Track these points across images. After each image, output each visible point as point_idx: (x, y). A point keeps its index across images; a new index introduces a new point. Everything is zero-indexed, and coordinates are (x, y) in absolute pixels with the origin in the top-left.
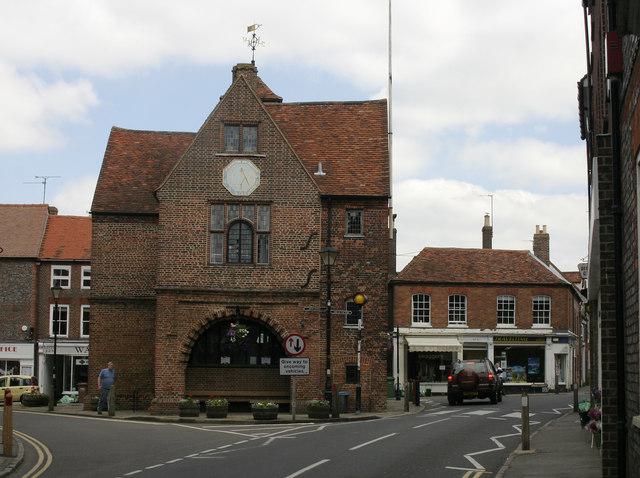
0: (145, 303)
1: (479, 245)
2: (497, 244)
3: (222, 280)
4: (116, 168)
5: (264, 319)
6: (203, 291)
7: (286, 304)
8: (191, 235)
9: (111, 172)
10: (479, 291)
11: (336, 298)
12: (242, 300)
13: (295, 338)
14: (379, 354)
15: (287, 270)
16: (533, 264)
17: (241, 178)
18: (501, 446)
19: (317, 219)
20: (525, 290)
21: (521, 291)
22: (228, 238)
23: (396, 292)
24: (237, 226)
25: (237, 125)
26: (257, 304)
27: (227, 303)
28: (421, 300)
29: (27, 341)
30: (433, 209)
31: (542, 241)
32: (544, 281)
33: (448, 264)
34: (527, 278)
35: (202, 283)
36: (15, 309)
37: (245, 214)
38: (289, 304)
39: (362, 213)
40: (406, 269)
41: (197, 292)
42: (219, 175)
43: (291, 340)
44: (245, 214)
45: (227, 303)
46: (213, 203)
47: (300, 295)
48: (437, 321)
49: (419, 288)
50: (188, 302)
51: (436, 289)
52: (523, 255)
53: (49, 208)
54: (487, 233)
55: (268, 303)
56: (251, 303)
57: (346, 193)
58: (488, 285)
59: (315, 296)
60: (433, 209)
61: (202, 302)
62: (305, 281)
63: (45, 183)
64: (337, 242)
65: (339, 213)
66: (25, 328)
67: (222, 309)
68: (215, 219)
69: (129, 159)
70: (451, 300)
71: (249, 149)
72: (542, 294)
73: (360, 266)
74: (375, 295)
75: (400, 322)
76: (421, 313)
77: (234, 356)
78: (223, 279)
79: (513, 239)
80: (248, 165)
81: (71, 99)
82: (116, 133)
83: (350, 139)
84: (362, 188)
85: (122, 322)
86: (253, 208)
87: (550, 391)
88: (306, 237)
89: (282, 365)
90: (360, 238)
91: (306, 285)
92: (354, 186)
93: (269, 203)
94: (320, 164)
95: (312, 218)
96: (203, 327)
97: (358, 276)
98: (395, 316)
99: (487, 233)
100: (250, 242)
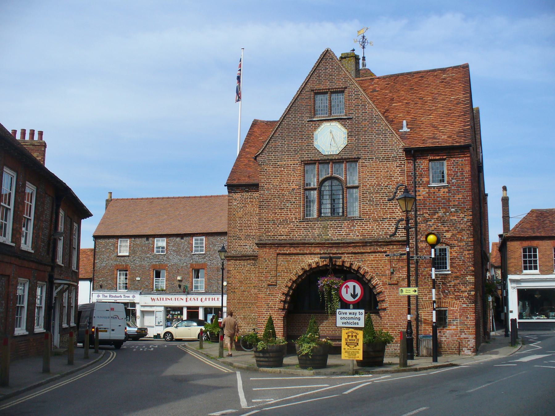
3: (315, 233)
6: (298, 244)
7: (375, 252)
9: (248, 153)
15: (375, 220)
17: (330, 138)
19: (402, 171)
23: (508, 246)
24: (327, 183)
27: (320, 254)
38: (378, 252)
39: (445, 163)
40: (517, 226)
41: (292, 245)
42: (310, 137)
43: (347, 287)
44: (340, 172)
45: (320, 254)
48: (544, 269)
56: (342, 253)
65: (423, 163)
67: (317, 260)
74: (461, 240)
76: (530, 262)
78: (317, 232)
83: (434, 99)
89: (338, 316)
90: (444, 187)
91: (394, 235)
94: (405, 122)
95: (397, 172)
97: (443, 223)
98: (508, 265)
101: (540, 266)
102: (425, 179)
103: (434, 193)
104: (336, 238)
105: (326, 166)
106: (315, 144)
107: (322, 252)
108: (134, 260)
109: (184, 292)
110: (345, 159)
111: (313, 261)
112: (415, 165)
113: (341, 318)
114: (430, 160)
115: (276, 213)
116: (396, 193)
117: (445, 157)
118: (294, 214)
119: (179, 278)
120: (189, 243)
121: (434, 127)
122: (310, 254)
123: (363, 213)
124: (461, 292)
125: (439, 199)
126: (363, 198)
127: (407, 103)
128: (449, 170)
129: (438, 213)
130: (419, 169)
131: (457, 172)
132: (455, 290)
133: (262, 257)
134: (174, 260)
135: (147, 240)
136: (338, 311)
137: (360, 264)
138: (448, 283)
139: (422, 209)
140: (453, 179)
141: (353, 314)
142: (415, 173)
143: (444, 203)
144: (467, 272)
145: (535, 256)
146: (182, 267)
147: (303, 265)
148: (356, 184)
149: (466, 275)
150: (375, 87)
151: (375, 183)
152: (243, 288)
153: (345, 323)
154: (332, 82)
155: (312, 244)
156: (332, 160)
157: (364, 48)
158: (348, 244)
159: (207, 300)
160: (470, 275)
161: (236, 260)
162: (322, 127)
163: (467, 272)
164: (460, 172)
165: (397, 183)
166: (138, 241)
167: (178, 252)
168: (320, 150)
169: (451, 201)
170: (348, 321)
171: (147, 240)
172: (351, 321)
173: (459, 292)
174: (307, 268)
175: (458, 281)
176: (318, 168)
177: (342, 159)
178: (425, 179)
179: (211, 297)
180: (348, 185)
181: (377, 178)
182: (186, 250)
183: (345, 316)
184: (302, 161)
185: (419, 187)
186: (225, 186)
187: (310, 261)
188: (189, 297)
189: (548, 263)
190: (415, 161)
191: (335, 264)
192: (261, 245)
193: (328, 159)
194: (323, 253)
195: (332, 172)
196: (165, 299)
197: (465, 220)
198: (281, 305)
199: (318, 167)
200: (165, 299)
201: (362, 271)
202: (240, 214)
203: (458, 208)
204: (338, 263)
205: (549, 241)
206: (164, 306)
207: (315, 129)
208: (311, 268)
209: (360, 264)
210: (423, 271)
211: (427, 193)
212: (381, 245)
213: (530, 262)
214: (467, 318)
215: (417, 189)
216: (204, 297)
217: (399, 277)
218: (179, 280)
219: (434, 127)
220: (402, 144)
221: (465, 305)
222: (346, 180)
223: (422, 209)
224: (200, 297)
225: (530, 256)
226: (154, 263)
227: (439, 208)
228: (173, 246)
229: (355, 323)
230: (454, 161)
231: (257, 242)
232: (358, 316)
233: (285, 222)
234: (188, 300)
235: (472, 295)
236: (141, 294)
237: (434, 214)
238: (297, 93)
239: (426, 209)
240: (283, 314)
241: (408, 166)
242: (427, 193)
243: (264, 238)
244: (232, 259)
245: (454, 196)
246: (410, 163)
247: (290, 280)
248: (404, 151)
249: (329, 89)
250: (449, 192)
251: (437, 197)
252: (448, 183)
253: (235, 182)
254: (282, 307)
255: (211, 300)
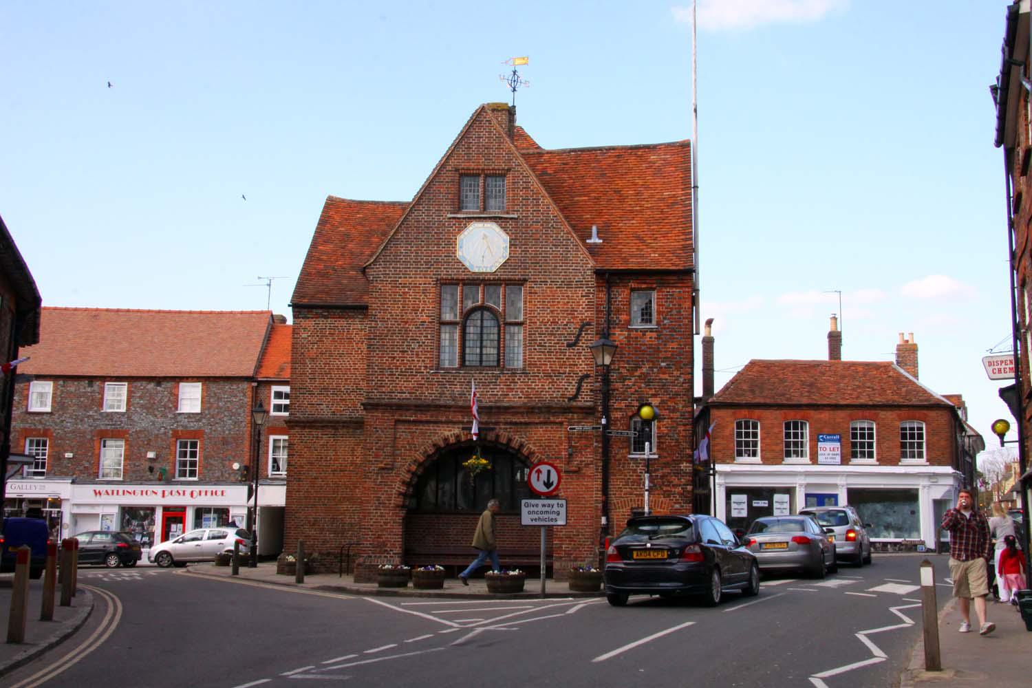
1: (823, 355)
2: (849, 354)
4: (330, 247)
6: (429, 406)
7: (545, 423)
8: (412, 327)
9: (322, 253)
10: (825, 415)
11: (618, 415)
13: (544, 468)
14: (681, 494)
16: (899, 380)
17: (482, 247)
18: (879, 655)
20: (889, 413)
21: (883, 414)
24: (478, 315)
26: (506, 423)
28: (747, 427)
29: (240, 482)
30: (754, 309)
31: (908, 353)
32: (914, 401)
33: (782, 381)
34: (890, 397)
35: (429, 395)
36: (225, 442)
39: (654, 295)
40: (727, 388)
42: (451, 243)
43: (539, 472)
45: (462, 423)
47: (566, 410)
48: (768, 455)
49: (745, 412)
50: (409, 421)
51: (767, 413)
52: (883, 368)
53: (272, 315)
54: (835, 340)
55: (521, 423)
56: (497, 423)
57: (631, 266)
58: (836, 407)
59: (588, 412)
60: (754, 309)
61: (428, 422)
62: (572, 390)
63: (270, 285)
64: (619, 336)
65: (621, 294)
66: (236, 466)
67: (457, 431)
69: (346, 238)
70: (788, 427)
71: (495, 208)
72: (913, 418)
73: (651, 368)
74: (675, 410)
75: (720, 455)
76: (747, 444)
77: (450, 502)
79: (868, 346)
80: (492, 229)
81: (770, 530)
82: (333, 207)
84: (653, 258)
85: (331, 453)
87: (929, 550)
89: (524, 510)
90: (651, 330)
91: (575, 398)
92: (642, 256)
94: (594, 229)
95: (582, 301)
97: (648, 383)
99: (835, 340)
100: (496, 337)
101: (762, 451)
102: (623, 317)
103: (637, 338)
105: (474, 288)
106: (459, 254)
108: (62, 421)
109: (160, 480)
110: (504, 280)
111: (452, 432)
112: (609, 295)
113: (529, 513)
115: (394, 358)
117: (655, 286)
118: (423, 361)
119: (151, 455)
120: (171, 393)
121: (638, 238)
123: (529, 364)
124: (674, 486)
125: (643, 348)
126: (530, 342)
127: (595, 198)
128: (660, 305)
130: (616, 301)
132: (663, 483)
133: (371, 425)
134: (143, 422)
135: (91, 385)
136: (523, 502)
137: (523, 440)
140: (664, 318)
141: (549, 506)
142: (609, 308)
143: (650, 355)
144: (682, 457)
145: (755, 435)
146: (157, 436)
148: (521, 319)
149: (681, 462)
150: (546, 168)
153: (536, 520)
154: (486, 159)
155: (450, 407)
156: (484, 280)
157: (514, 90)
158: (507, 410)
159: (203, 494)
160: (687, 462)
162: (471, 228)
165: (582, 320)
166: (72, 387)
167: (150, 408)
168: (467, 264)
169: (661, 351)
170: (541, 516)
171: (91, 385)
172: (546, 516)
173: (669, 486)
174: (442, 444)
175: (666, 471)
176: (462, 292)
177: (499, 279)
178: (623, 317)
179: (210, 488)
180: (509, 320)
181: (552, 311)
182: (165, 406)
183: (535, 509)
184: (438, 280)
186: (289, 306)
187: (447, 433)
188: (168, 488)
189: (774, 447)
190: (609, 289)
191: (485, 439)
192: (370, 406)
193: (478, 279)
195: (484, 298)
196: (121, 492)
197: (682, 380)
198: (400, 500)
199: (462, 290)
200: (121, 492)
201: (525, 451)
202: (313, 353)
203: (671, 361)
204: (489, 438)
205: (778, 412)
206: (120, 505)
208: (448, 444)
210: (617, 454)
211: (625, 338)
212: (555, 412)
213: (747, 444)
216: (197, 488)
217: (581, 461)
218: (150, 459)
219: (638, 238)
220: (591, 263)
221: (677, 506)
222: (505, 313)
224: (189, 489)
225: (747, 435)
226: (103, 427)
227: (642, 361)
228: (140, 398)
229: (552, 520)
231: (364, 401)
232: (556, 509)
234: (166, 493)
235: (689, 492)
236: (73, 482)
237: (635, 369)
238: (433, 173)
239: (624, 361)
240: (402, 513)
242: (625, 338)
243: (376, 395)
245: (665, 345)
246: (602, 291)
247: (415, 461)
248: (594, 273)
249: (483, 170)
250: (658, 338)
251: (640, 345)
252: (658, 324)
253: (305, 301)
254: (401, 503)
255: (209, 494)
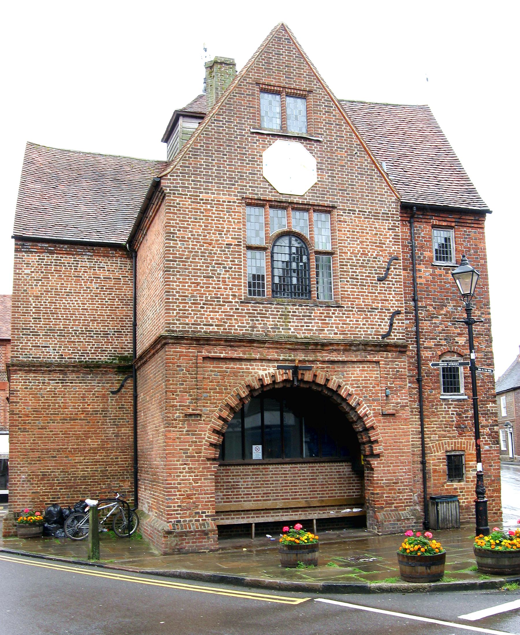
0: (129, 367)
1: (278, 422)
5: (332, 385)
12: (301, 356)
15: (361, 310)
22: (272, 257)
24: (285, 241)
25: (278, 93)
26: (323, 362)
27: (277, 360)
37: (298, 222)
41: (232, 342)
42: (256, 160)
44: (298, 222)
45: (277, 360)
46: (252, 203)
50: (219, 359)
55: (338, 362)
56: (312, 362)
61: (240, 360)
62: (386, 329)
65: (423, 229)
67: (272, 370)
68: (258, 226)
78: (270, 322)
82: (31, 146)
86: (306, 215)
88: (383, 261)
91: (388, 334)
93: (328, 210)
95: (387, 236)
96: (241, 399)
103: (441, 275)
104: (303, 336)
107: (281, 358)
111: (267, 372)
114: (434, 227)
115: (198, 284)
116: (388, 269)
118: (231, 289)
122: (261, 360)
129: (446, 306)
130: (419, 237)
131: (469, 248)
137: (341, 380)
138: (464, 413)
139: (425, 298)
144: (488, 398)
147: (249, 379)
151: (359, 251)
152: (41, 423)
161: (30, 371)
163: (488, 398)
164: (473, 248)
174: (256, 385)
181: (361, 242)
185: (420, 264)
187: (261, 373)
194: (285, 360)
207: (264, 148)
209: (341, 380)
214: (491, 466)
215: (418, 267)
217: (398, 403)
223: (425, 298)
227: (447, 299)
230: (465, 231)
233: (217, 301)
239: (430, 299)
241: (402, 231)
244: (20, 370)
251: (445, 282)
253: (29, 234)
